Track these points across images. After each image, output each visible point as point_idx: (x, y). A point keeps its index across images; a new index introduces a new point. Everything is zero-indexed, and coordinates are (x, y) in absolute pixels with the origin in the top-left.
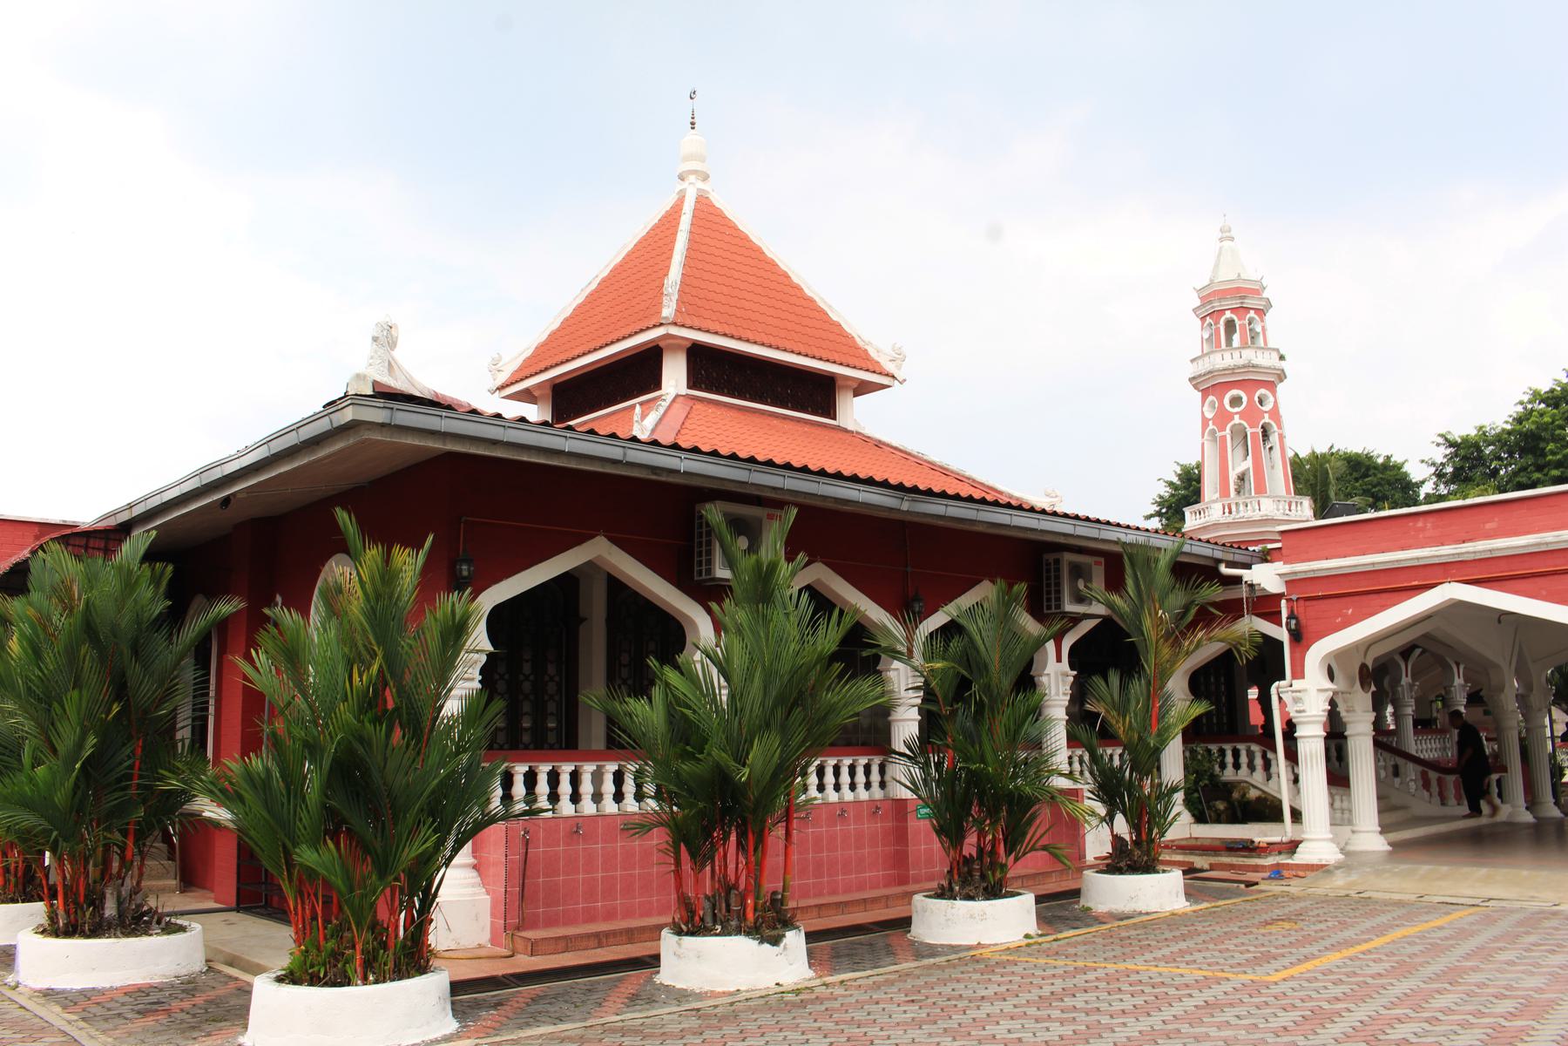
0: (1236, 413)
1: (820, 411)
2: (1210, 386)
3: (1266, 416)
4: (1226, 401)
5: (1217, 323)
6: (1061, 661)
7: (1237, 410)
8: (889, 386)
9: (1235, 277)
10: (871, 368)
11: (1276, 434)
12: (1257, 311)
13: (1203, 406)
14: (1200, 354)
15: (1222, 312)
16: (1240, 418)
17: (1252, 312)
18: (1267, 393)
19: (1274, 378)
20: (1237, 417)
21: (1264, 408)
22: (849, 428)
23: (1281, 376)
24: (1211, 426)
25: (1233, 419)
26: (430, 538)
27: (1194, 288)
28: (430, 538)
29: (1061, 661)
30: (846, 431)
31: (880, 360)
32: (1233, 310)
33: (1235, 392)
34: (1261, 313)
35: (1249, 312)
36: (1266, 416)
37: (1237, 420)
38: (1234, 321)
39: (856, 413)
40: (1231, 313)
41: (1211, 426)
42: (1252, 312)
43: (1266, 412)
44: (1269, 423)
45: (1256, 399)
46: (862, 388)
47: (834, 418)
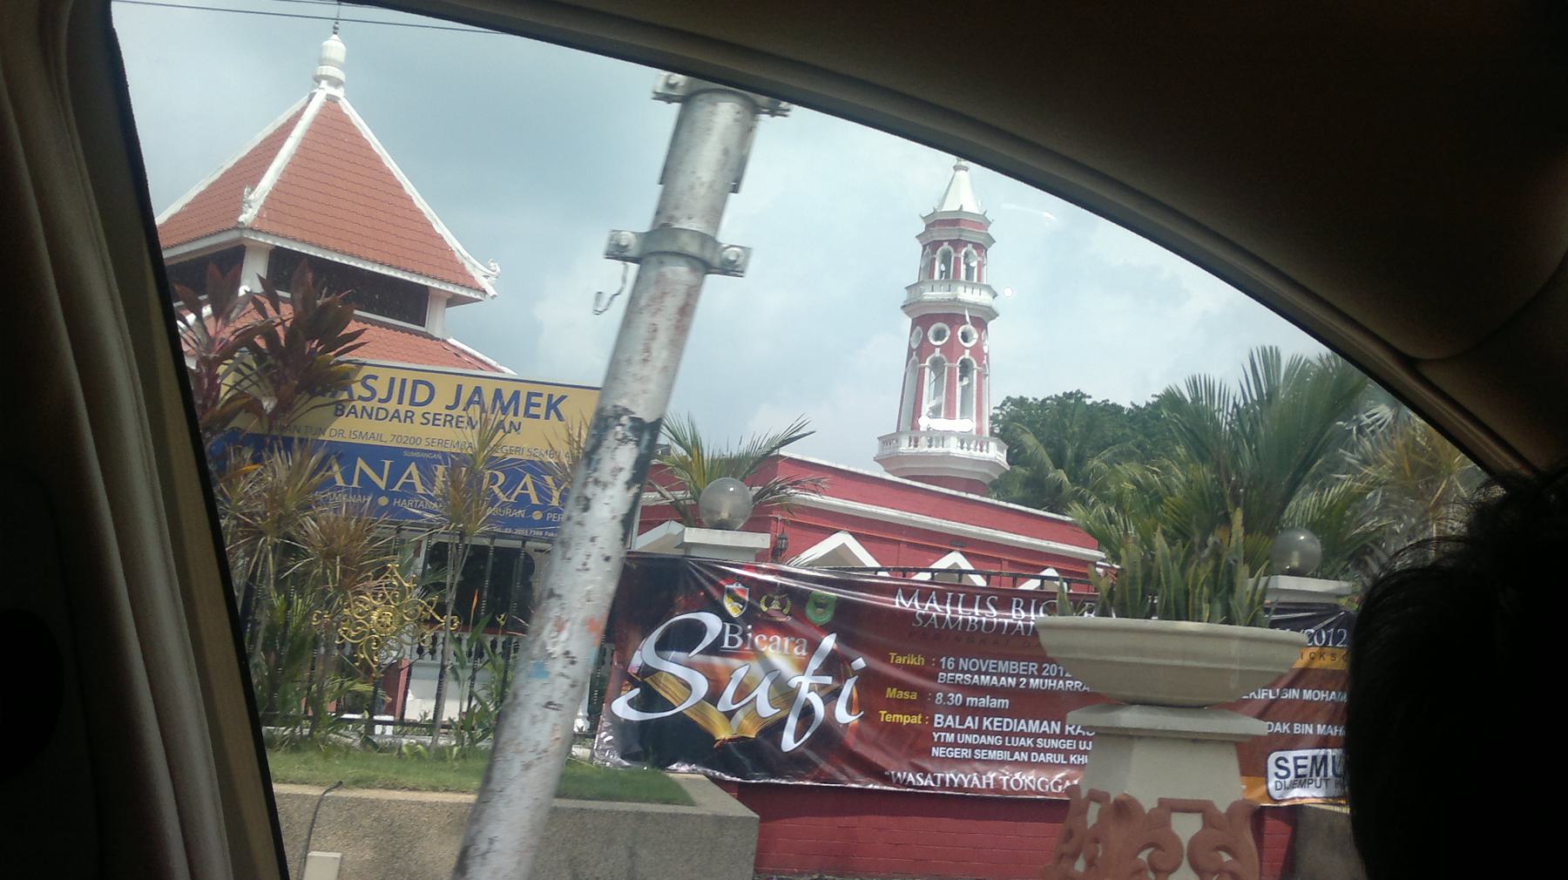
0: (938, 346)
1: (407, 317)
2: (924, 319)
3: (967, 352)
4: (931, 333)
5: (934, 252)
6: (549, 395)
7: (939, 343)
8: (480, 300)
9: (957, 208)
10: (461, 281)
11: (975, 372)
12: (977, 246)
13: (911, 335)
14: (916, 281)
15: (940, 243)
16: (971, 354)
17: (970, 246)
18: (947, 328)
19: (982, 319)
20: (938, 350)
21: (966, 345)
22: (436, 336)
23: (992, 314)
24: (914, 357)
25: (964, 354)
26: (283, 343)
27: (920, 215)
28: (283, 343)
29: (549, 395)
30: (432, 338)
31: (474, 275)
32: (951, 242)
33: (940, 325)
34: (981, 248)
35: (942, 245)
36: (967, 352)
37: (937, 352)
38: (950, 252)
39: (441, 322)
40: (973, 247)
41: (914, 357)
42: (970, 246)
43: (967, 348)
44: (968, 359)
45: (959, 334)
46: (454, 301)
47: (424, 326)
